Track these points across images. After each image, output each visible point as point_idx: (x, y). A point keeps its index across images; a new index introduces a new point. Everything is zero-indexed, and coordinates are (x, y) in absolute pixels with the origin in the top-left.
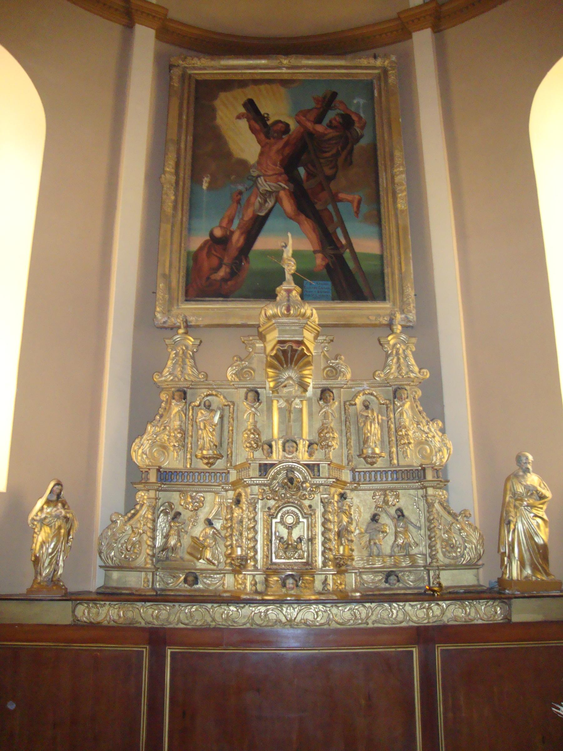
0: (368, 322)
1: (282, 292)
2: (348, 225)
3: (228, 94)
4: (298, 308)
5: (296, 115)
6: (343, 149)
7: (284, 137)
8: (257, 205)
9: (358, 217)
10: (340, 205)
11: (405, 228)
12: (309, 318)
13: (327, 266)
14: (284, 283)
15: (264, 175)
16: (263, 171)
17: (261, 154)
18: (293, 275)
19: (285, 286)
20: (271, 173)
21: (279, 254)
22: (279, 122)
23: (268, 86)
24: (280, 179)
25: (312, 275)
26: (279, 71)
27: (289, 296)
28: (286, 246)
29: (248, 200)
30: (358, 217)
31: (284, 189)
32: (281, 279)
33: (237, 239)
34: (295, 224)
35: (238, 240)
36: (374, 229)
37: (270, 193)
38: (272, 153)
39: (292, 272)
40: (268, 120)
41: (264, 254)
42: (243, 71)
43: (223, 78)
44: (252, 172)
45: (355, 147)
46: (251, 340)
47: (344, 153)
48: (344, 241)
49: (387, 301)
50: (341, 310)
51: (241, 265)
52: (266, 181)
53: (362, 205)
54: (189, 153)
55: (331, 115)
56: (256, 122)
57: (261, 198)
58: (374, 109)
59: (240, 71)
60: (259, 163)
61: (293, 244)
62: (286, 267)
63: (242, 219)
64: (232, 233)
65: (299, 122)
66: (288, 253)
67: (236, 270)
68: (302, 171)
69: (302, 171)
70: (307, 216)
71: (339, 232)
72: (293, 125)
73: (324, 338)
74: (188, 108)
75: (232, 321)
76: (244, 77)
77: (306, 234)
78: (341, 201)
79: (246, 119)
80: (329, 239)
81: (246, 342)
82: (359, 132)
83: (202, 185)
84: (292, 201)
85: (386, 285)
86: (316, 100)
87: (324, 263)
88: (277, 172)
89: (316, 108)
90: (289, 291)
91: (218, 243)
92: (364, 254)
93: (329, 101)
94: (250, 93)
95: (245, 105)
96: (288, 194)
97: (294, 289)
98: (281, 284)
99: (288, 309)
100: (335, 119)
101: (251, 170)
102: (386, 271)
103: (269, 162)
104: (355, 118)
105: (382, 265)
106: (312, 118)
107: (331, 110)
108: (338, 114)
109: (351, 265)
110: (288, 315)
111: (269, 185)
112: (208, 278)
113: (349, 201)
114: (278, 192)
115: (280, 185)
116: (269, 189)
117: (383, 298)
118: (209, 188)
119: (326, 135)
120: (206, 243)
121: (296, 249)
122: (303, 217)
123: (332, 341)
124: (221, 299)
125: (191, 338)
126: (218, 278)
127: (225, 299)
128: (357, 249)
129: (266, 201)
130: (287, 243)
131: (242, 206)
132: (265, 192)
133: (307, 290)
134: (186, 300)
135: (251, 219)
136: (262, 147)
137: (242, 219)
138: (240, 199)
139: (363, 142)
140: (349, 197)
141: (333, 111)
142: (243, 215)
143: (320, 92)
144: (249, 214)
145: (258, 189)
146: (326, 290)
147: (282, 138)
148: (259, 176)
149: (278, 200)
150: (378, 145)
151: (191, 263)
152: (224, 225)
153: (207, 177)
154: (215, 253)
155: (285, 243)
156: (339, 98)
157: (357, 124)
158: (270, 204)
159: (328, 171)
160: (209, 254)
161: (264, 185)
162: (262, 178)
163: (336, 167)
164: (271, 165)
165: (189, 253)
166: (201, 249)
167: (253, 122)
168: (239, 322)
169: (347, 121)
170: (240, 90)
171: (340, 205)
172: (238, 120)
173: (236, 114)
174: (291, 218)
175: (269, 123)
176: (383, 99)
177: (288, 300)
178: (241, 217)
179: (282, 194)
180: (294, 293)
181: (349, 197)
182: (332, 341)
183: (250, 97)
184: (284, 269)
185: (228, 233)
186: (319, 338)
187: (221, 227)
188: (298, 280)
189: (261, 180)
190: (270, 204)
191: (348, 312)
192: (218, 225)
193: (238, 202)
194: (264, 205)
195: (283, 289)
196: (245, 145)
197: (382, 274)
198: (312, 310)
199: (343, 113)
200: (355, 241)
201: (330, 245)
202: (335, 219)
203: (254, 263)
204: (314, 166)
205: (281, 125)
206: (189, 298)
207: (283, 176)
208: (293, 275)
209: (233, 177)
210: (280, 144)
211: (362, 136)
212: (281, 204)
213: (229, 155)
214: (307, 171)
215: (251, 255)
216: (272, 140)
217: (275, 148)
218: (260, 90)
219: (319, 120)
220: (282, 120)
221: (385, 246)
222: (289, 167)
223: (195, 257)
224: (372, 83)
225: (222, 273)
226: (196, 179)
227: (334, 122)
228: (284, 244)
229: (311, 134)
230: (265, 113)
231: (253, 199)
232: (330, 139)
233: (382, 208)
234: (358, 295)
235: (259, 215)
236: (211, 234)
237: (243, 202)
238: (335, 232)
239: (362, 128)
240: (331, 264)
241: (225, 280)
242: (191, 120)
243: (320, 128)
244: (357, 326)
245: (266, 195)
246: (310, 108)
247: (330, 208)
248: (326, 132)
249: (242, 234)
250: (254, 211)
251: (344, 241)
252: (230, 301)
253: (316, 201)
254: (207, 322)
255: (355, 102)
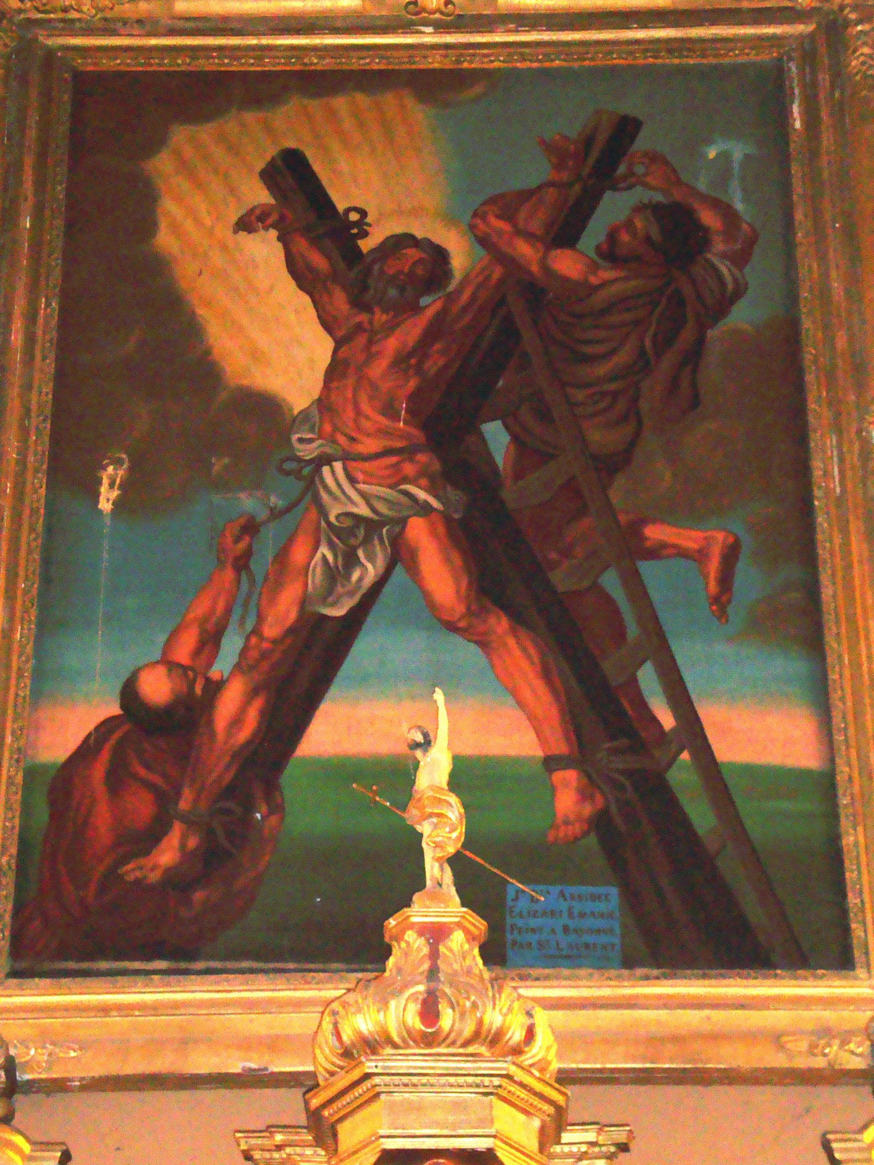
0: (779, 1061)
1: (410, 935)
2: (687, 653)
3: (205, 132)
4: (475, 1005)
5: (475, 215)
6: (663, 343)
7: (424, 301)
8: (316, 577)
9: (722, 615)
10: (650, 571)
11: (384, 1068)
12: (517, 1051)
13: (600, 823)
14: (416, 897)
15: (346, 458)
16: (342, 440)
17: (335, 372)
18: (455, 861)
19: (421, 911)
20: (369, 445)
21: (398, 775)
22: (407, 240)
23: (362, 99)
24: (409, 469)
25: (538, 859)
26: (409, 40)
27: (434, 954)
28: (427, 743)
29: (282, 557)
30: (722, 615)
31: (425, 509)
32: (402, 876)
33: (235, 713)
34: (467, 653)
35: (237, 721)
36: (792, 665)
37: (372, 526)
38: (378, 369)
39: (451, 850)
40: (364, 234)
41: (347, 772)
42: (265, 41)
43: (181, 64)
44: (297, 445)
45: (712, 334)
46: (279, 1148)
47: (668, 361)
48: (667, 720)
49: (861, 972)
50: (665, 1006)
51: (246, 821)
52: (352, 481)
53: (741, 566)
54: (46, 366)
55: (613, 208)
56: (315, 242)
57: (331, 545)
58: (786, 173)
59: (253, 41)
60: (323, 404)
61: (453, 732)
62: (425, 828)
63: (256, 631)
64: (214, 688)
65: (483, 241)
66: (434, 770)
67: (225, 846)
68: (496, 436)
69: (496, 436)
70: (518, 618)
71: (648, 679)
72: (461, 256)
73: (591, 1136)
74: (40, 184)
75: (203, 1063)
76: (269, 65)
77: (515, 693)
78: (654, 553)
79: (273, 233)
80: (607, 712)
81: (257, 1155)
82: (728, 279)
83: (96, 496)
84: (457, 559)
85: (852, 900)
86: (556, 151)
87: (587, 810)
88: (399, 444)
89: (551, 184)
90: (436, 934)
91: (153, 734)
92: (751, 771)
93: (605, 153)
94: (289, 125)
95: (269, 176)
96: (441, 530)
97: (459, 925)
98: (408, 904)
99: (429, 1011)
100: (629, 224)
101: (295, 437)
102: (848, 840)
103: (363, 398)
104: (708, 218)
105: (833, 815)
106: (537, 225)
107: (614, 188)
108: (639, 209)
109: (701, 816)
110: (429, 1040)
111: (362, 494)
112: (112, 876)
113: (683, 554)
114: (403, 522)
115: (406, 493)
116: (363, 511)
117: (841, 958)
118: (119, 505)
119: (594, 289)
120: (106, 727)
121: (467, 750)
122: (499, 624)
123: (624, 1148)
124: (162, 964)
125: (19, 1140)
126: (154, 877)
127: (183, 965)
128: (724, 751)
129: (351, 561)
130: (433, 725)
131: (259, 578)
132: (349, 522)
133: (520, 923)
134: (15, 974)
135: (292, 631)
136: (339, 344)
137: (256, 631)
138: (248, 554)
139: (742, 316)
140: (686, 538)
141: (625, 195)
142: (260, 618)
143: (568, 122)
144: (283, 611)
145: (323, 512)
146: (600, 923)
147: (416, 309)
148: (328, 460)
149: (401, 555)
150: (807, 323)
151: (42, 815)
152: (183, 653)
153: (118, 463)
154: (143, 772)
155: (426, 735)
156: (643, 142)
157: (719, 245)
158: (369, 571)
159: (601, 437)
160: (117, 779)
161: (345, 494)
162: (338, 466)
163: (632, 414)
164: (374, 415)
165: (32, 774)
166: (86, 752)
167: (301, 245)
168: (236, 1068)
169: (678, 233)
170: (250, 117)
171: (650, 571)
172: (243, 234)
173: (234, 214)
174: (451, 627)
175: (366, 245)
176: (827, 140)
177: (433, 973)
178: (249, 625)
179: (419, 532)
180: (457, 939)
181: (686, 538)
182: (624, 1148)
183: (291, 144)
184: (421, 835)
185: (198, 690)
186: (566, 1137)
187: (166, 661)
188: (475, 884)
189: (333, 475)
190: (369, 571)
191: (692, 1018)
192: (157, 655)
193: (242, 563)
194: (348, 577)
195: (412, 926)
196: (275, 338)
197: (835, 858)
198: (529, 1014)
199: (659, 198)
200: (711, 714)
201: (613, 738)
202: (633, 631)
203: (305, 812)
204: (544, 414)
205: (412, 253)
206: (23, 965)
207: (422, 457)
208: (455, 861)
209: (219, 464)
210: (411, 331)
211: (739, 293)
212: (413, 570)
213: (205, 372)
214: (515, 438)
215: (291, 777)
216: (381, 317)
217: (392, 344)
218: (332, 114)
219: (565, 233)
220: (419, 234)
221: (839, 738)
222: (443, 426)
223: (60, 788)
224: (779, 72)
225: (167, 855)
226: (70, 472)
227: (625, 238)
228: (419, 738)
229: (534, 291)
230: (348, 210)
231: (299, 554)
232: (610, 308)
233: (825, 577)
234: (736, 946)
235: (325, 617)
236: (129, 694)
237: (262, 563)
238: (634, 681)
239: (741, 259)
240: (614, 809)
241: (178, 883)
242: (55, 235)
243: (567, 264)
244: (730, 1077)
245: (352, 535)
246: (534, 183)
247: (611, 582)
248: (594, 280)
249: (253, 692)
250: (304, 602)
251: (667, 720)
252: (199, 973)
253: (554, 556)
254: (99, 1068)
255: (712, 154)
